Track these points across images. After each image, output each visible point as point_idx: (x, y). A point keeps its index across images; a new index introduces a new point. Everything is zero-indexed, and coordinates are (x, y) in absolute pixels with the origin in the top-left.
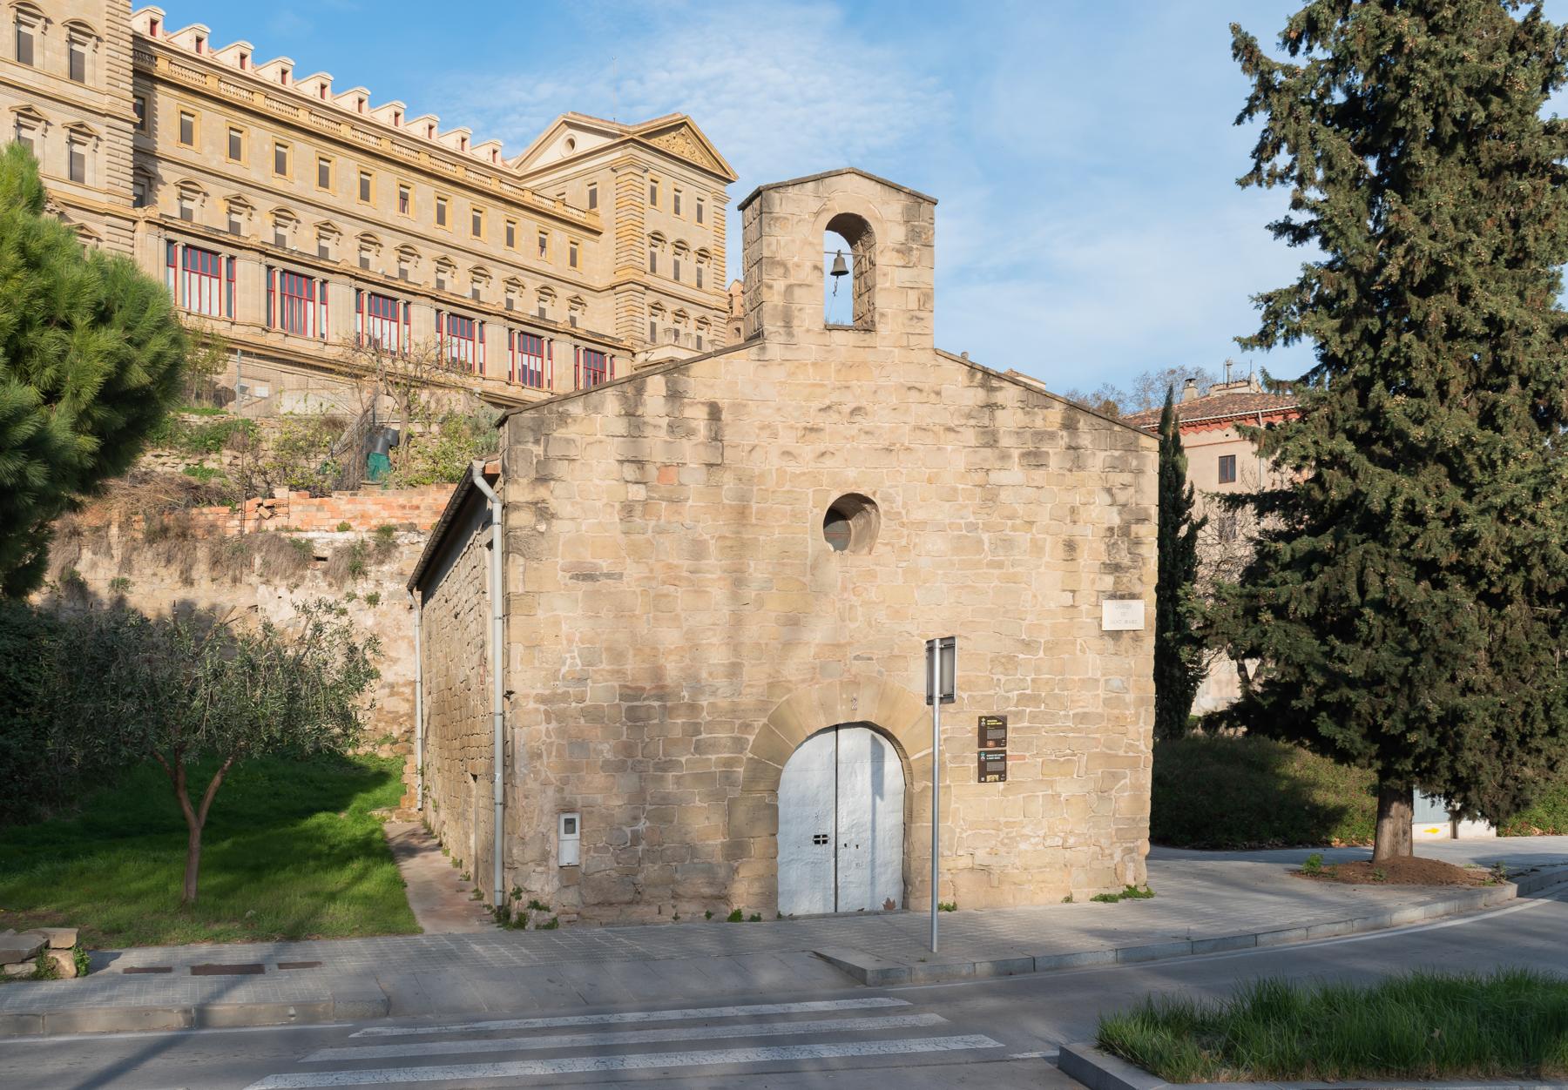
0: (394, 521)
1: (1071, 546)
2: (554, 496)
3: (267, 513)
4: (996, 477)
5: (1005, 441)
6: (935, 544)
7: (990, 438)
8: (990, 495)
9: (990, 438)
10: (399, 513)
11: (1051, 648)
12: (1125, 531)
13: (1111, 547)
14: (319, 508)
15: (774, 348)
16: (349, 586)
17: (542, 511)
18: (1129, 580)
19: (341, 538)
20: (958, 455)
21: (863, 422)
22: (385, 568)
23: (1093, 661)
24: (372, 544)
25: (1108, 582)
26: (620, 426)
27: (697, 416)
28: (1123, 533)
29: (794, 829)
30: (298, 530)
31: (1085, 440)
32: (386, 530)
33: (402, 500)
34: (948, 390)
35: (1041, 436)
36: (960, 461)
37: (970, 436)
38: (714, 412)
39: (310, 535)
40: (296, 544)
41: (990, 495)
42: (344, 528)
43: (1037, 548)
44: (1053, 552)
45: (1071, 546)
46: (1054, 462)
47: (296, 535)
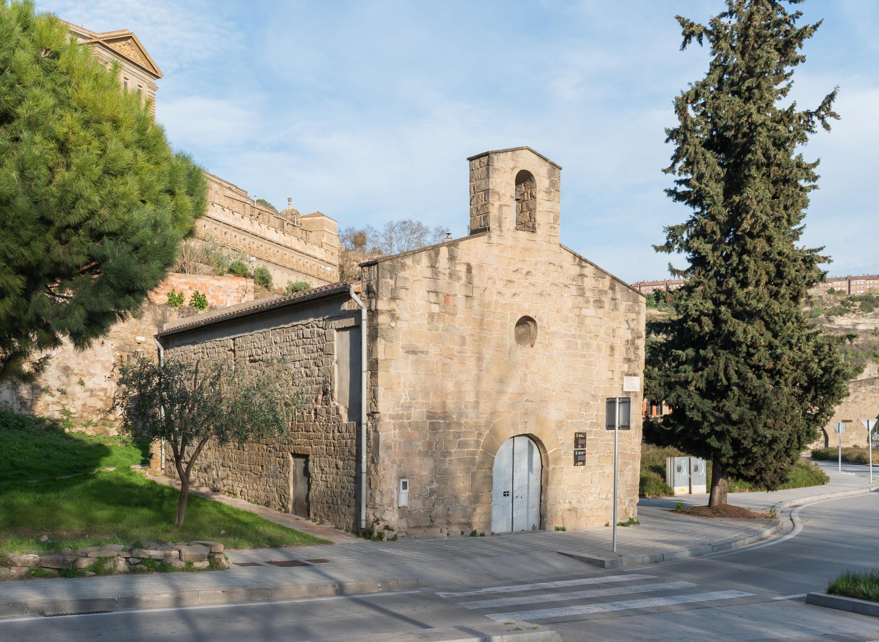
1: (612, 348)
4: (585, 312)
6: (559, 344)
9: (582, 292)
13: (628, 349)
17: (393, 316)
20: (569, 298)
21: (531, 279)
25: (625, 367)
26: (428, 273)
27: (462, 269)
37: (574, 290)
41: (581, 320)
43: (599, 349)
44: (606, 351)
45: (612, 348)
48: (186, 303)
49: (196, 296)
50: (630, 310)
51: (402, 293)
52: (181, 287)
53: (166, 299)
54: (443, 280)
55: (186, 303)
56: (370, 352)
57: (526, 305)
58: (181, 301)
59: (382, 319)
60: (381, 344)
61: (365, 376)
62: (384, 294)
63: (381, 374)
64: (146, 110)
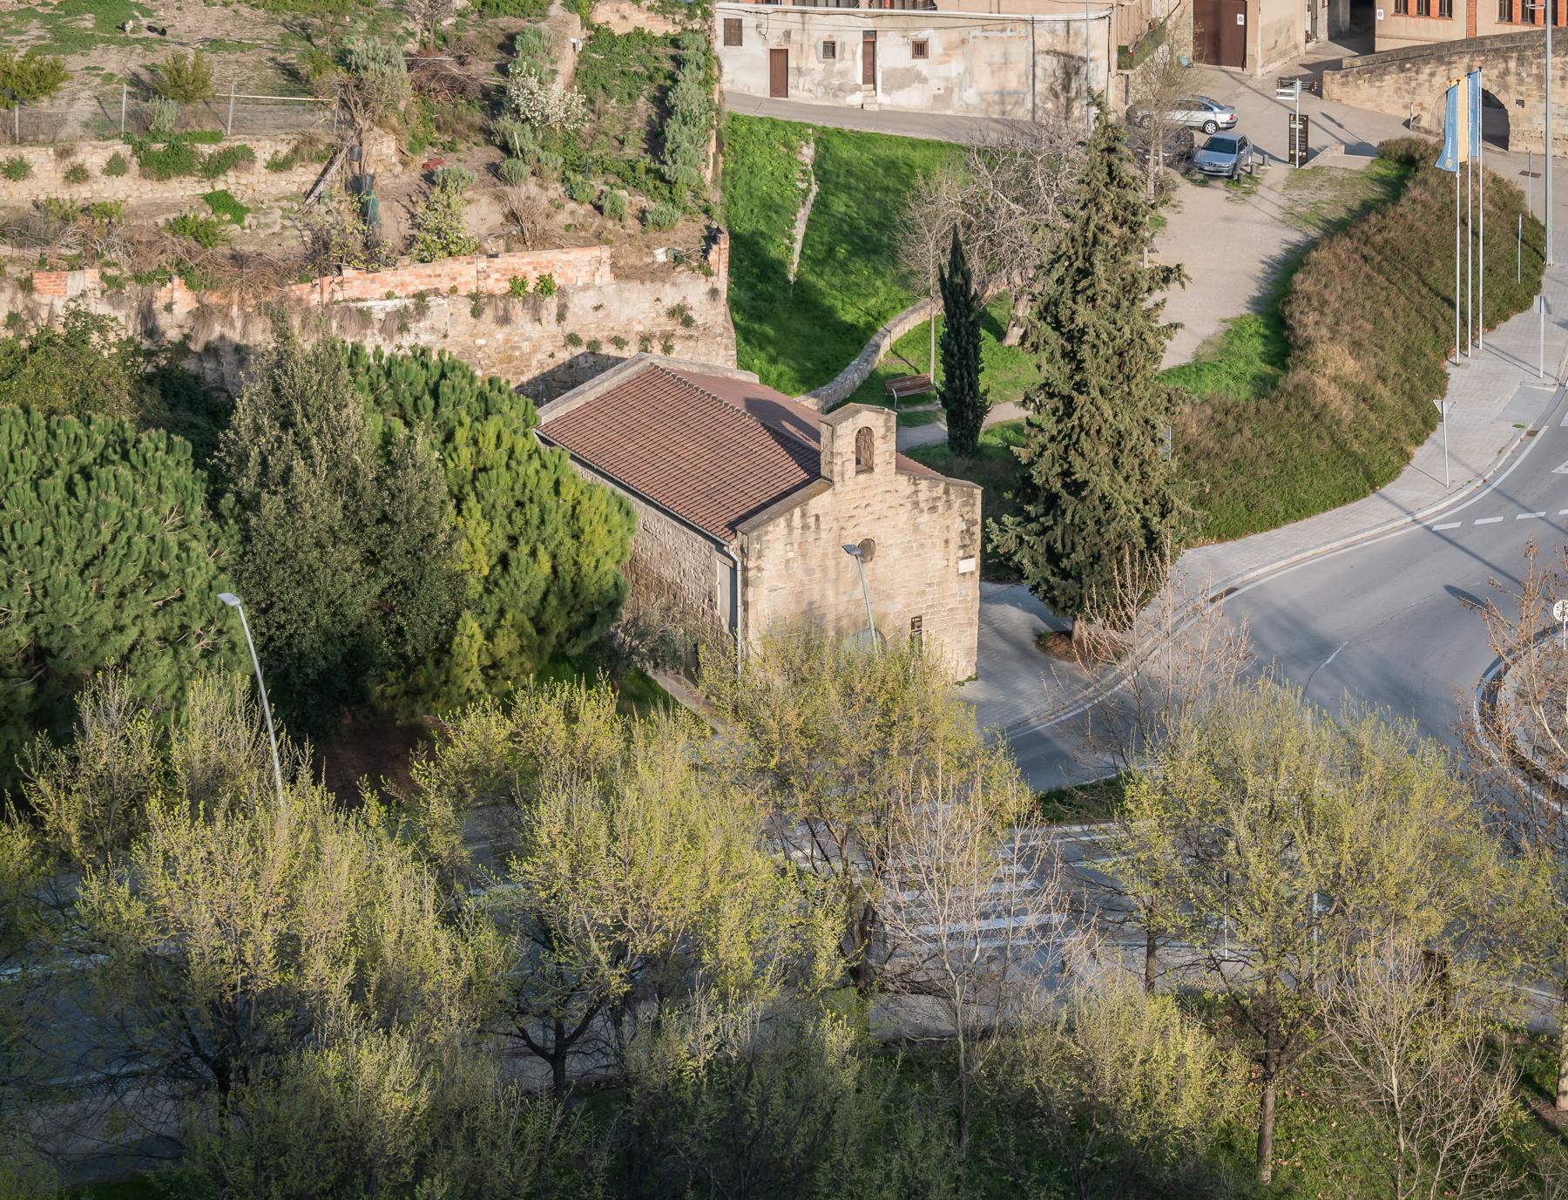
0: (422, 288)
1: (947, 542)
2: (763, 563)
3: (337, 288)
4: (920, 520)
5: (922, 505)
6: (896, 552)
7: (916, 504)
8: (916, 528)
9: (916, 504)
10: (427, 280)
11: (939, 584)
12: (968, 530)
13: (962, 539)
14: (373, 281)
15: (838, 486)
16: (397, 339)
17: (759, 569)
18: (970, 551)
19: (391, 305)
20: (904, 514)
21: (869, 509)
22: (422, 324)
23: (954, 586)
24: (412, 307)
25: (961, 553)
26: (785, 531)
27: (812, 520)
28: (968, 532)
29: (762, 530)
30: (359, 300)
31: (952, 497)
32: (420, 297)
33: (428, 271)
34: (900, 488)
35: (936, 499)
36: (905, 518)
37: (909, 506)
38: (817, 517)
39: (369, 304)
40: (360, 311)
41: (916, 528)
42: (389, 296)
43: (934, 544)
44: (939, 542)
45: (947, 542)
46: (940, 510)
47: (360, 305)
48: (530, 289)
49: (541, 278)
50: (965, 504)
51: (766, 552)
52: (524, 268)
53: (508, 286)
54: (797, 532)
55: (530, 289)
56: (743, 594)
57: (865, 531)
58: (523, 284)
59: (751, 574)
60: (750, 591)
61: (740, 610)
62: (753, 555)
63: (751, 611)
64: (628, 729)
